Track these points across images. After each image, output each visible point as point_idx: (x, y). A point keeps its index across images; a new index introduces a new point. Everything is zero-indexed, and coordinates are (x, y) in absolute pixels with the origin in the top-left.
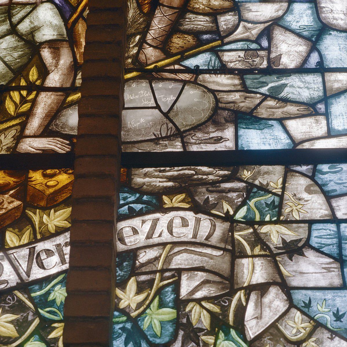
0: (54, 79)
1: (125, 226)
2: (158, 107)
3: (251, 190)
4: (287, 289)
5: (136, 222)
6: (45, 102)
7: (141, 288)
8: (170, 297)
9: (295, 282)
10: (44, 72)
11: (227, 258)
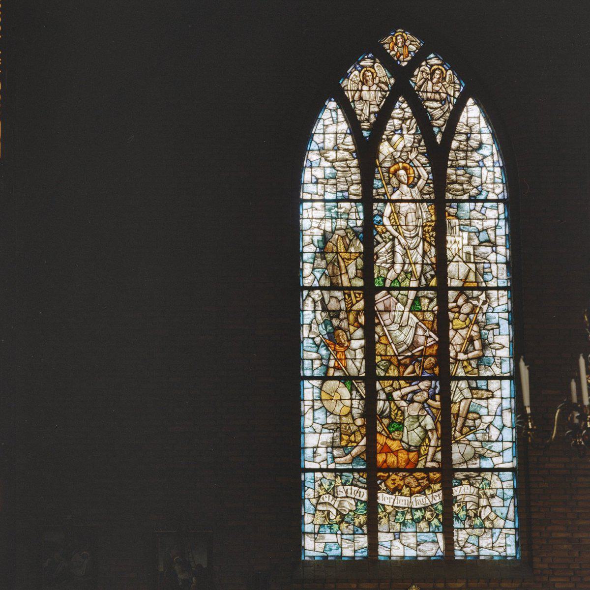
0: (433, 443)
1: (454, 489)
2: (460, 453)
3: (484, 479)
4: (491, 507)
5: (456, 488)
6: (431, 450)
7: (459, 506)
8: (465, 509)
9: (492, 505)
10: (430, 441)
11: (478, 499)
